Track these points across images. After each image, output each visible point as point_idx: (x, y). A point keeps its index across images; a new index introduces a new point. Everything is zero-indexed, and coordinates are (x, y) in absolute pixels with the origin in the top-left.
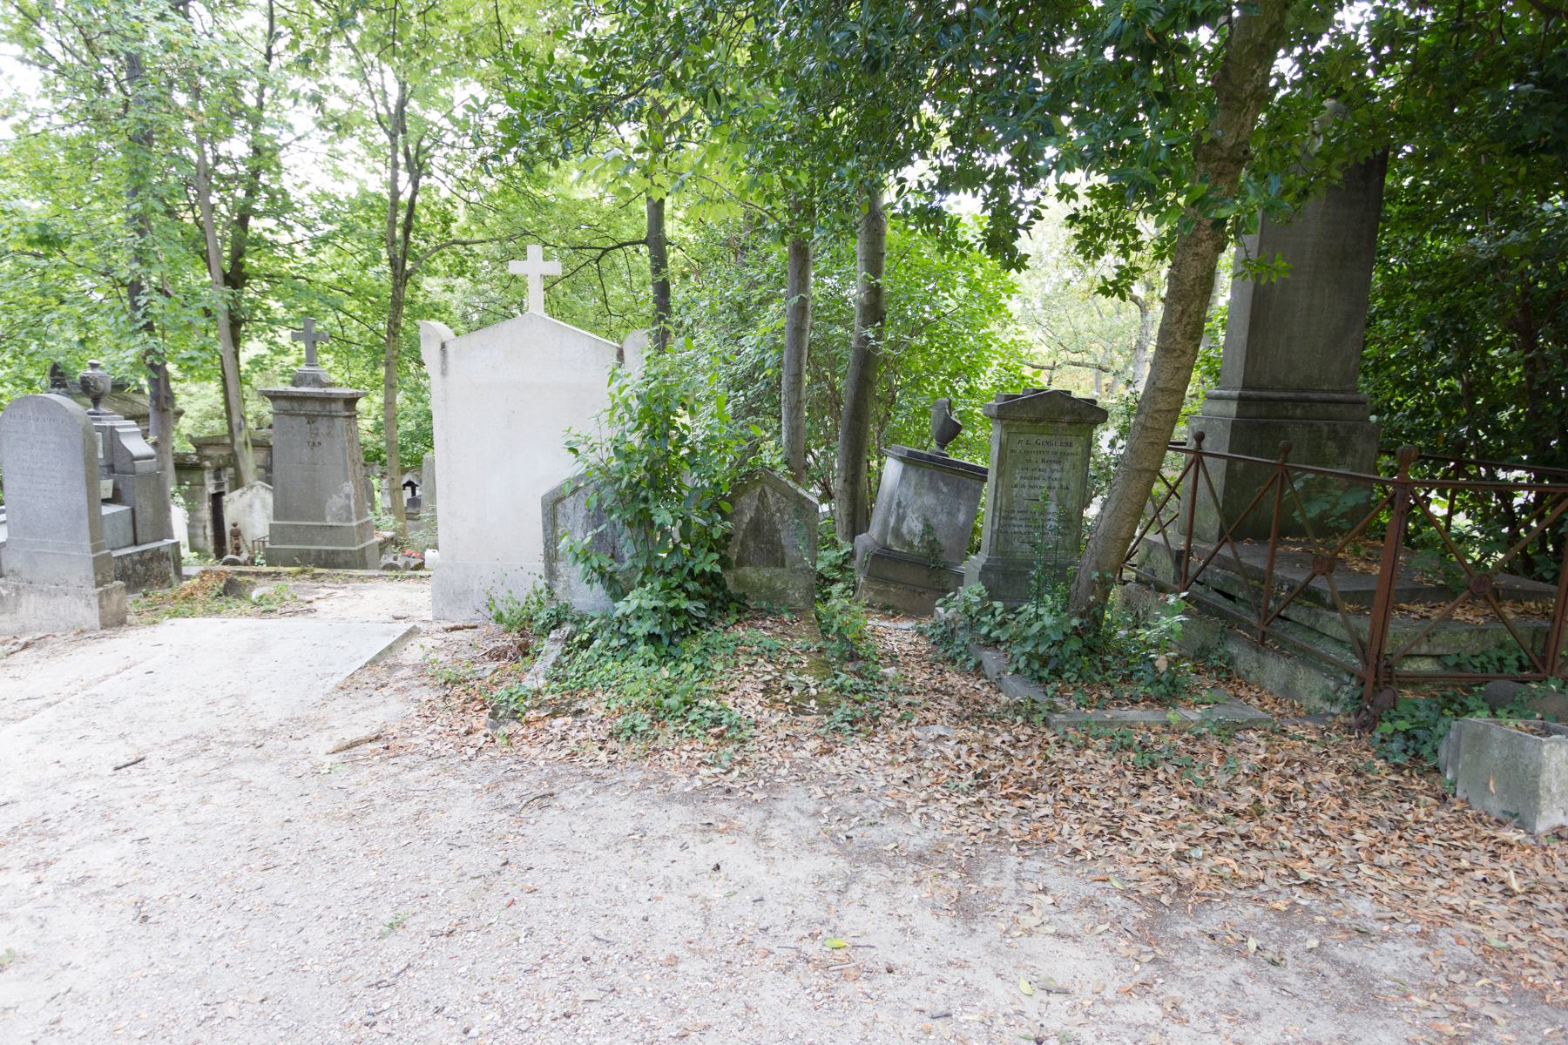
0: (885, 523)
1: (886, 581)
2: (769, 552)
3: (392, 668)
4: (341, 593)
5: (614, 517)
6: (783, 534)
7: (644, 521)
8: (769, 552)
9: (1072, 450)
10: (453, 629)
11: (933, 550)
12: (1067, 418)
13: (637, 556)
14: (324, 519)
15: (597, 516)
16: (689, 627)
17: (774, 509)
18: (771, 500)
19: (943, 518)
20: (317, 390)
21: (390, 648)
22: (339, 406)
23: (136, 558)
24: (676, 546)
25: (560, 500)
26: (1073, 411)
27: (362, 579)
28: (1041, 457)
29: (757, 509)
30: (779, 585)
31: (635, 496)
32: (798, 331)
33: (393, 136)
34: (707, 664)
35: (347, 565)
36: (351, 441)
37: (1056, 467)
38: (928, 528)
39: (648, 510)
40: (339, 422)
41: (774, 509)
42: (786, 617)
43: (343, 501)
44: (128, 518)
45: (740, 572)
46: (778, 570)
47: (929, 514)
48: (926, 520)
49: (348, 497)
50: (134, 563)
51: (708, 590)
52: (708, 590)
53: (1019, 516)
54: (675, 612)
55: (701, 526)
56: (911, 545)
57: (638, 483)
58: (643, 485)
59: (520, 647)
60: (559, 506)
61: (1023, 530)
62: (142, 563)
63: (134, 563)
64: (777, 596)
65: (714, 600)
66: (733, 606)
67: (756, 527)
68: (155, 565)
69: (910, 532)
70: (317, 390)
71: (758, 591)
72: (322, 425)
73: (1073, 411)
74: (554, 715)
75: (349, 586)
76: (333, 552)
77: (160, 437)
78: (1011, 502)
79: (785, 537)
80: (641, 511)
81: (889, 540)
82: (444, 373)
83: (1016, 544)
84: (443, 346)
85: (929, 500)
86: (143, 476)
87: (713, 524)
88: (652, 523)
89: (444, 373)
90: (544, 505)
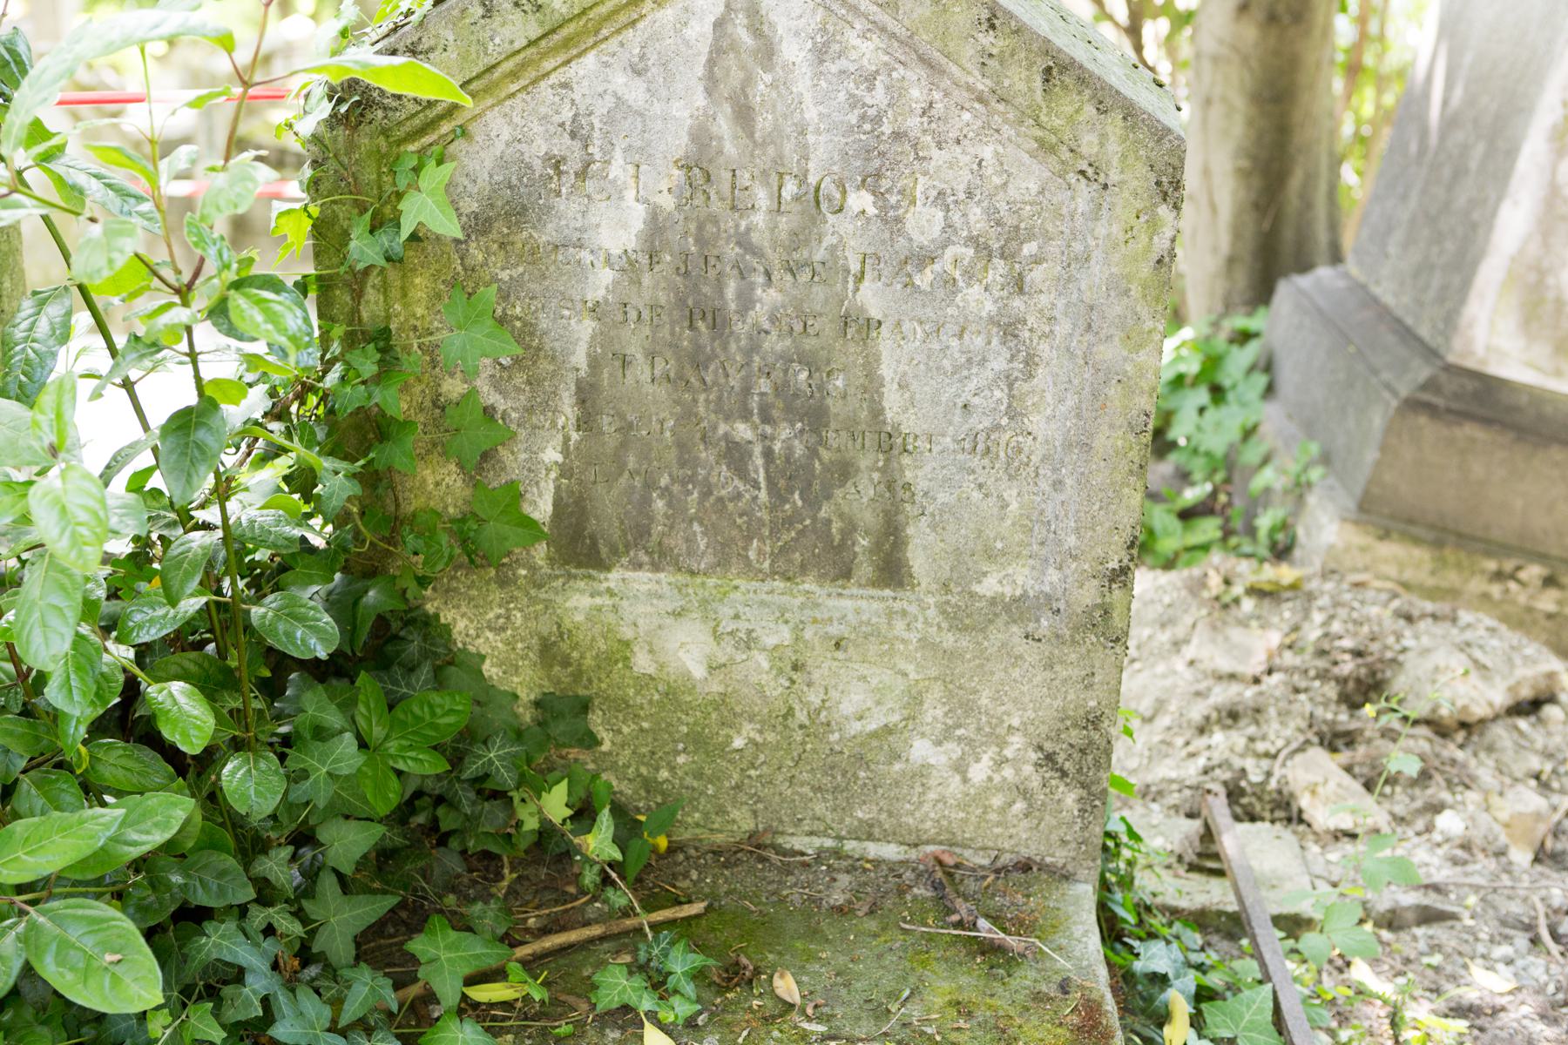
2: (789, 476)
7: (1143, 999)
8: (789, 476)
29: (698, 167)
45: (579, 602)
46: (855, 605)
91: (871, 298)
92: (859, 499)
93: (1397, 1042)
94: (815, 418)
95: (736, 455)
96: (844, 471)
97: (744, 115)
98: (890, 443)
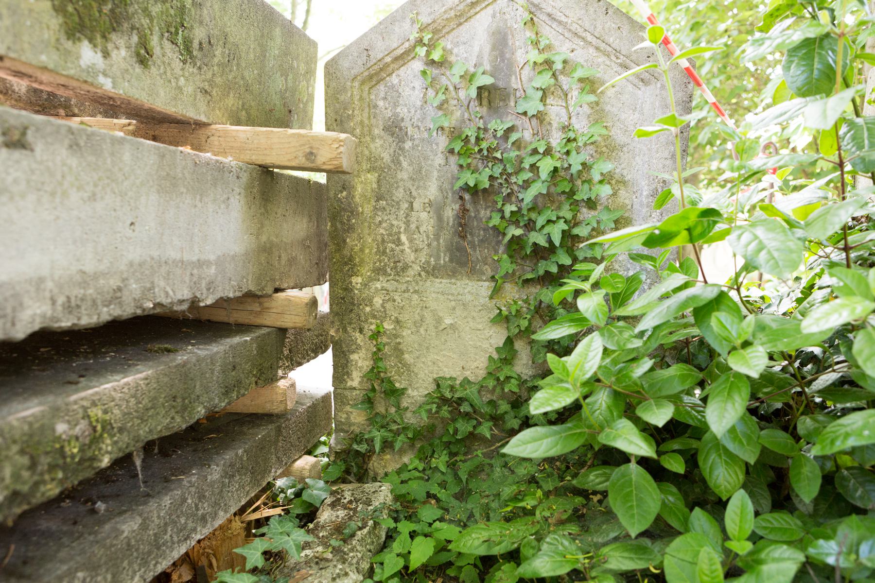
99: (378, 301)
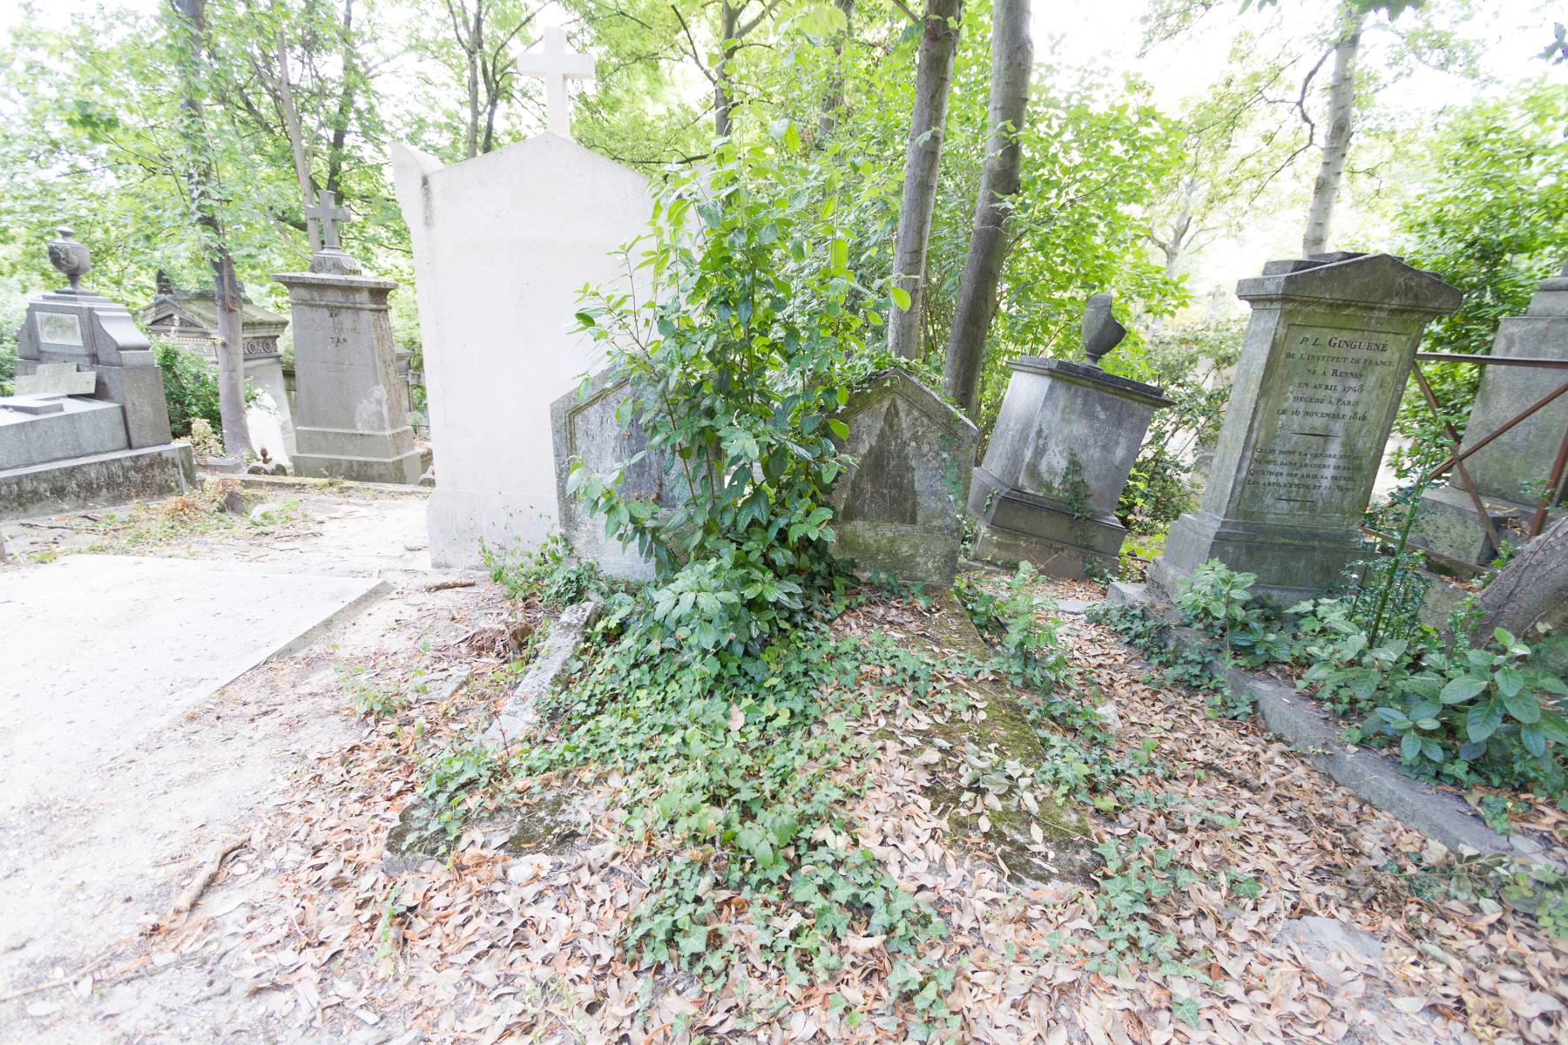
0: (1016, 457)
1: (1015, 533)
2: (894, 500)
3: (311, 663)
4: (363, 511)
5: (657, 439)
6: (918, 475)
7: (708, 447)
8: (894, 500)
9: (1385, 356)
10: (438, 588)
11: (1077, 495)
12: (1395, 303)
13: (693, 501)
14: (354, 427)
15: (636, 435)
16: (783, 626)
17: (907, 435)
18: (904, 421)
19: (1096, 453)
20: (343, 277)
21: (328, 624)
22: (363, 298)
23: (128, 464)
24: (757, 491)
25: (578, 410)
26: (1409, 288)
27: (392, 495)
28: (1332, 366)
29: (882, 436)
30: (905, 549)
31: (694, 407)
32: (923, 188)
33: (471, 53)
34: (813, 710)
35: (381, 478)
36: (381, 339)
37: (1353, 383)
38: (1075, 466)
39: (714, 430)
40: (366, 317)
41: (907, 435)
42: (921, 603)
43: (373, 407)
44: (119, 411)
45: (848, 527)
47: (1077, 448)
48: (1073, 455)
49: (379, 402)
50: (126, 470)
51: (804, 560)
52: (804, 560)
53: (1280, 458)
54: (754, 605)
55: (799, 459)
56: (1049, 487)
57: (699, 386)
58: (707, 389)
59: (514, 635)
60: (578, 419)
61: (1283, 480)
62: (138, 470)
63: (126, 470)
64: (898, 564)
65: (812, 576)
66: (839, 582)
67: (877, 462)
68: (157, 471)
69: (1051, 470)
70: (343, 277)
71: (873, 557)
72: (346, 318)
73: (1409, 288)
74: (516, 846)
75: (376, 503)
76: (366, 463)
77: (229, 337)
78: (1271, 436)
79: (921, 480)
80: (702, 431)
81: (1023, 480)
82: (428, 222)
83: (1269, 500)
84: (425, 182)
85: (1080, 428)
86: (134, 368)
87: (820, 459)
88: (719, 453)
89: (428, 222)
90: (555, 416)
91: (913, 463)
92: (909, 504)
93: (1556, 887)
94: (901, 489)
95: (883, 496)
96: (906, 499)
97: (891, 426)
98: (915, 493)
99: (299, 32)
